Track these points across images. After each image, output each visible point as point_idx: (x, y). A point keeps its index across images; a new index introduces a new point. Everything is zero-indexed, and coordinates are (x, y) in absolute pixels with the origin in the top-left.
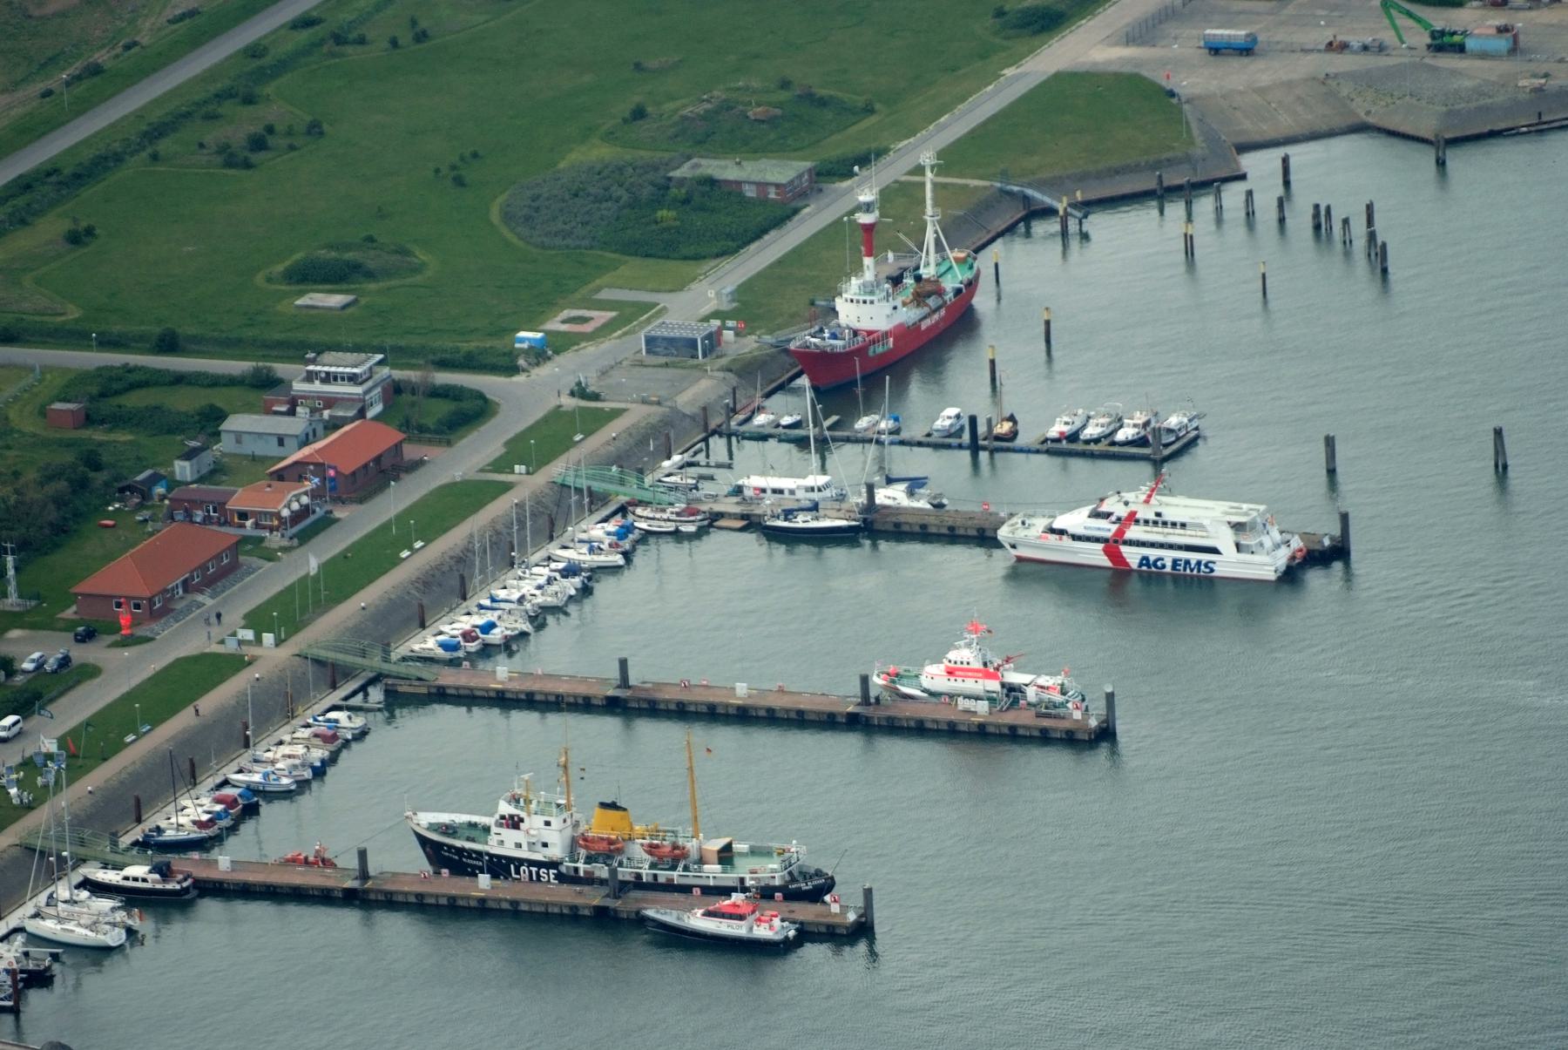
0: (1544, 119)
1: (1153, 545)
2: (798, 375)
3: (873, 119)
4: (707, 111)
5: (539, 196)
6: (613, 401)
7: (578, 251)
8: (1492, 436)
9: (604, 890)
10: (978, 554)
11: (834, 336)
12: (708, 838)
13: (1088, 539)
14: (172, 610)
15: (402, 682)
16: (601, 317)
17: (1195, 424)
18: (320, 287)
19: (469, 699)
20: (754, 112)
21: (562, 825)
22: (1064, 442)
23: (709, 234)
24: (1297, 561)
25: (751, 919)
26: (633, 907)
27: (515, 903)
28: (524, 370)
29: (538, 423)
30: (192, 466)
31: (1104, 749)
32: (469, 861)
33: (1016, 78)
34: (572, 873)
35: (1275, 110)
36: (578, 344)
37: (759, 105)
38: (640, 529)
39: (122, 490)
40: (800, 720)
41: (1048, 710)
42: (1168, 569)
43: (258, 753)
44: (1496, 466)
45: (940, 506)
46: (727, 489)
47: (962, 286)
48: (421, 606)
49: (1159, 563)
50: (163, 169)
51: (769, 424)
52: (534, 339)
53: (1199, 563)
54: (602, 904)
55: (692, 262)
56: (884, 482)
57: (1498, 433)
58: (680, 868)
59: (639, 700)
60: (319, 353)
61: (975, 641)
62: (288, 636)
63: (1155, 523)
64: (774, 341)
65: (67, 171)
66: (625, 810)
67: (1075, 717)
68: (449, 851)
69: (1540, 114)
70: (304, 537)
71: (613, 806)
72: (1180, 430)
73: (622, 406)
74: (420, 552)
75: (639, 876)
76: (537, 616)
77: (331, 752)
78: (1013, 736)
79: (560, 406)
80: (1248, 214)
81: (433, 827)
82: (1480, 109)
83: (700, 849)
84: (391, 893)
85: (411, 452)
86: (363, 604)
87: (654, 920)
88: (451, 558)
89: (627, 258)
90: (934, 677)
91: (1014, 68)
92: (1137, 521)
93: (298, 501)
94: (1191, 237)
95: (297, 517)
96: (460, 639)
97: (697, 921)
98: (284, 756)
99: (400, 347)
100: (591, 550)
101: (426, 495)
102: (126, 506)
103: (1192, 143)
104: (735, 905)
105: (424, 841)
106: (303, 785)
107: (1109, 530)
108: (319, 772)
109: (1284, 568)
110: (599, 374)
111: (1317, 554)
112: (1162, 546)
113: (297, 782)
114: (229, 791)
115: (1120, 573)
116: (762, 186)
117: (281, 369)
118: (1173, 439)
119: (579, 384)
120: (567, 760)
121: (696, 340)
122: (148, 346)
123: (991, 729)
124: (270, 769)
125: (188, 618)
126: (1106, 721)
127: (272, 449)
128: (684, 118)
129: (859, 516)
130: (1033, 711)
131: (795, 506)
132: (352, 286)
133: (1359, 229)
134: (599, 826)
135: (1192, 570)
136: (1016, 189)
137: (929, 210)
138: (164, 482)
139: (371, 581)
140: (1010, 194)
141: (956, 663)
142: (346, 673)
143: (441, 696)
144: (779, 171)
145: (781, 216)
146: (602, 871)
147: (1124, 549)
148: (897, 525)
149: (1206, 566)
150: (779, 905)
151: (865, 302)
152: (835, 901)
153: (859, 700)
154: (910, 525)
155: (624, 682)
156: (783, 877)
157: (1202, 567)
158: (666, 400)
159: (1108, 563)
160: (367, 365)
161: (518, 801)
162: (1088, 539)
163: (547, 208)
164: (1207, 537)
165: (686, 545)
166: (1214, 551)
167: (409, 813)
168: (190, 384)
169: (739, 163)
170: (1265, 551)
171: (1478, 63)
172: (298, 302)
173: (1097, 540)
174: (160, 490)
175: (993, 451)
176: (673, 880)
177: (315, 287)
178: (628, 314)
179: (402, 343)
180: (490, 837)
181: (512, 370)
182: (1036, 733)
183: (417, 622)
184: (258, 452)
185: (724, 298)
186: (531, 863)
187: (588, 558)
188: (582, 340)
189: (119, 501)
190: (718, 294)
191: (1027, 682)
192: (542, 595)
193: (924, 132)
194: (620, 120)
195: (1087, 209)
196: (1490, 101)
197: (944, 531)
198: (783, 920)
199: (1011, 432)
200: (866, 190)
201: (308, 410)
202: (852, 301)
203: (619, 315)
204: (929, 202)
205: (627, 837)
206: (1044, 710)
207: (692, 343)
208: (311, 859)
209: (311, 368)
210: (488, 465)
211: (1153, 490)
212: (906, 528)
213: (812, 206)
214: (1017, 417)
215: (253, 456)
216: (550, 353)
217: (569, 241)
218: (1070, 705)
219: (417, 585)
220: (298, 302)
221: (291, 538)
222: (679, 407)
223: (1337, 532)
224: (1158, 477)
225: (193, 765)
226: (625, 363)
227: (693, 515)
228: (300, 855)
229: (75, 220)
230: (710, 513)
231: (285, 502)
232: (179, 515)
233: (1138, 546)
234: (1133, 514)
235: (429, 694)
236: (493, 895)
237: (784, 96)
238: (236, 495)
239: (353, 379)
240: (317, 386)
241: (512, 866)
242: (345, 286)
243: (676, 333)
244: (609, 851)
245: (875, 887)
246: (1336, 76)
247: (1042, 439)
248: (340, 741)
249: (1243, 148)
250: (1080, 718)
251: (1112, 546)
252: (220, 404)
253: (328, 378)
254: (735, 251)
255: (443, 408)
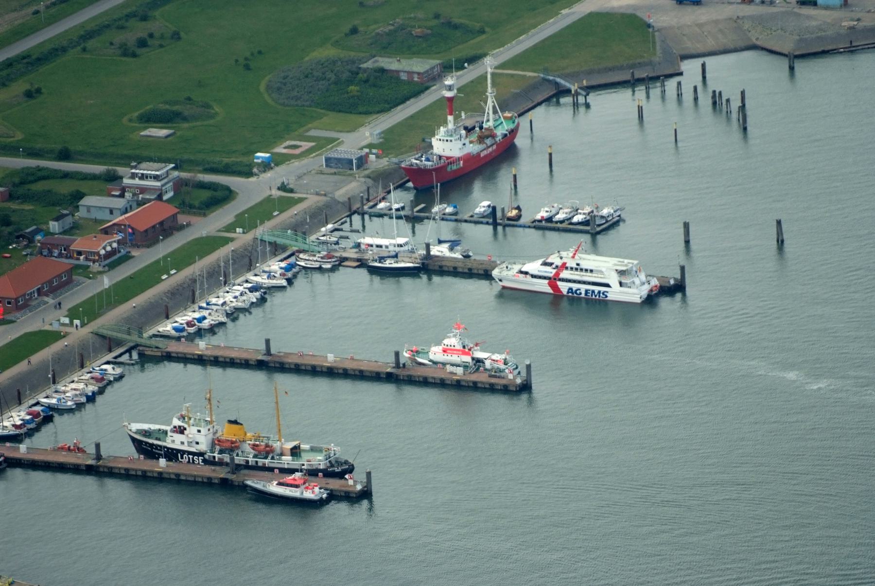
0: (854, 44)
1: (575, 281)
2: (408, 181)
3: (484, 37)
4: (390, 30)
5: (287, 76)
6: (301, 193)
7: (302, 108)
8: (775, 223)
9: (228, 469)
10: (484, 283)
11: (428, 160)
12: (287, 441)
13: (540, 277)
14: (30, 305)
15: (147, 349)
16: (306, 145)
17: (618, 214)
18: (157, 125)
19: (185, 359)
20: (417, 31)
21: (207, 432)
22: (544, 222)
23: (375, 100)
24: (654, 293)
25: (303, 487)
26: (240, 479)
27: (178, 475)
28: (256, 175)
29: (256, 205)
30: (59, 226)
31: (524, 397)
32: (157, 451)
33: (568, 15)
34: (212, 459)
35: (706, 36)
36: (290, 161)
37: (419, 27)
38: (299, 265)
39: (18, 237)
40: (360, 376)
41: (497, 373)
42: (583, 295)
43: (58, 387)
44: (778, 241)
45: (467, 257)
46: (352, 244)
47: (507, 132)
48: (167, 307)
49: (578, 292)
50: (88, 56)
51: (386, 208)
52: (265, 158)
53: (599, 292)
54: (224, 477)
55: (363, 116)
56: (437, 242)
57: (779, 223)
58: (269, 458)
59: (275, 362)
60: (139, 163)
61: (458, 334)
62: (89, 321)
63: (577, 269)
64: (397, 161)
65: (34, 57)
66: (242, 424)
67: (509, 378)
68: (146, 445)
69: (851, 42)
70: (112, 266)
71: (235, 422)
72: (608, 216)
73: (304, 196)
74: (174, 276)
75: (247, 462)
76: (232, 314)
77: (99, 387)
78: (475, 387)
79: (271, 196)
80: (678, 95)
81: (139, 432)
82: (818, 38)
83: (281, 448)
84: (112, 468)
85: (182, 219)
86: (134, 305)
87: (251, 487)
88: (190, 280)
89: (329, 113)
90: (436, 353)
91: (568, 9)
92: (567, 268)
93: (111, 246)
94: (642, 107)
95: (109, 255)
96: (185, 325)
97: (274, 488)
98: (72, 389)
99: (192, 160)
100: (269, 277)
101: (185, 244)
102: (18, 246)
103: (655, 54)
104: (294, 479)
105: (134, 440)
106: (80, 406)
107: (551, 273)
108: (91, 399)
109: (646, 296)
110: (297, 178)
111: (666, 288)
112: (579, 282)
113: (76, 404)
114: (38, 408)
115: (557, 296)
116: (410, 73)
117: (121, 170)
118: (604, 221)
119: (283, 183)
120: (210, 396)
121: (352, 160)
122: (54, 156)
123: (463, 383)
124: (63, 396)
125: (37, 310)
126: (526, 380)
127: (106, 215)
128: (378, 34)
129: (419, 261)
130: (487, 375)
131: (386, 254)
132: (174, 125)
133: (736, 104)
134: (227, 433)
135: (596, 296)
136: (551, 78)
137: (489, 90)
138: (42, 233)
139: (143, 292)
140: (549, 81)
141: (447, 346)
142: (119, 343)
143: (169, 357)
144: (419, 65)
145: (418, 89)
146: (226, 458)
147: (559, 283)
148: (441, 267)
149: (603, 294)
150: (321, 479)
151: (447, 141)
152: (351, 478)
153: (394, 365)
154: (448, 267)
155: (268, 352)
156: (325, 464)
157: (601, 295)
158: (329, 194)
159: (551, 291)
160: (165, 170)
161: (184, 419)
162: (540, 277)
163: (291, 83)
164: (604, 278)
165: (326, 275)
166: (608, 285)
167: (126, 424)
168: (72, 178)
169: (399, 61)
170: (636, 286)
171: (823, 12)
172: (142, 133)
173: (545, 278)
174: (39, 237)
175: (505, 226)
176: (265, 464)
177: (155, 125)
178: (322, 143)
179: (192, 158)
180: (167, 438)
181: (250, 174)
182: (487, 386)
183: (165, 316)
184: (98, 218)
185: (375, 136)
186: (190, 453)
187: (267, 281)
188: (292, 158)
189: (16, 243)
190: (371, 134)
191: (486, 357)
192: (236, 301)
193: (509, 45)
194: (343, 35)
195: (589, 90)
196: (823, 34)
197: (466, 271)
198: (320, 488)
199: (517, 215)
200: (449, 78)
201: (131, 195)
202: (440, 140)
203: (316, 145)
204: (489, 85)
205: (242, 440)
206: (493, 373)
207: (350, 162)
208: (72, 447)
209: (133, 171)
210: (223, 228)
211: (576, 251)
212: (446, 269)
213: (438, 85)
214: (521, 207)
215: (96, 219)
216: (273, 165)
217: (299, 102)
218: (507, 371)
219: (167, 294)
220: (142, 133)
221: (104, 267)
222: (336, 198)
223: (678, 276)
224: (594, 242)
225: (19, 393)
226: (313, 172)
227: (330, 258)
228: (66, 445)
229: (32, 84)
230: (340, 257)
231: (103, 245)
232: (45, 252)
233: (567, 282)
234: (564, 264)
235: (162, 356)
236: (167, 470)
237: (435, 22)
238: (76, 242)
239: (156, 178)
240: (137, 181)
241: (179, 455)
242: (170, 125)
243: (342, 156)
244: (231, 448)
245: (372, 471)
246: (743, 17)
247: (533, 220)
248: (105, 382)
249: (684, 57)
250: (512, 378)
251: (553, 281)
252: (83, 190)
253: (143, 177)
254: (389, 110)
255: (205, 195)
